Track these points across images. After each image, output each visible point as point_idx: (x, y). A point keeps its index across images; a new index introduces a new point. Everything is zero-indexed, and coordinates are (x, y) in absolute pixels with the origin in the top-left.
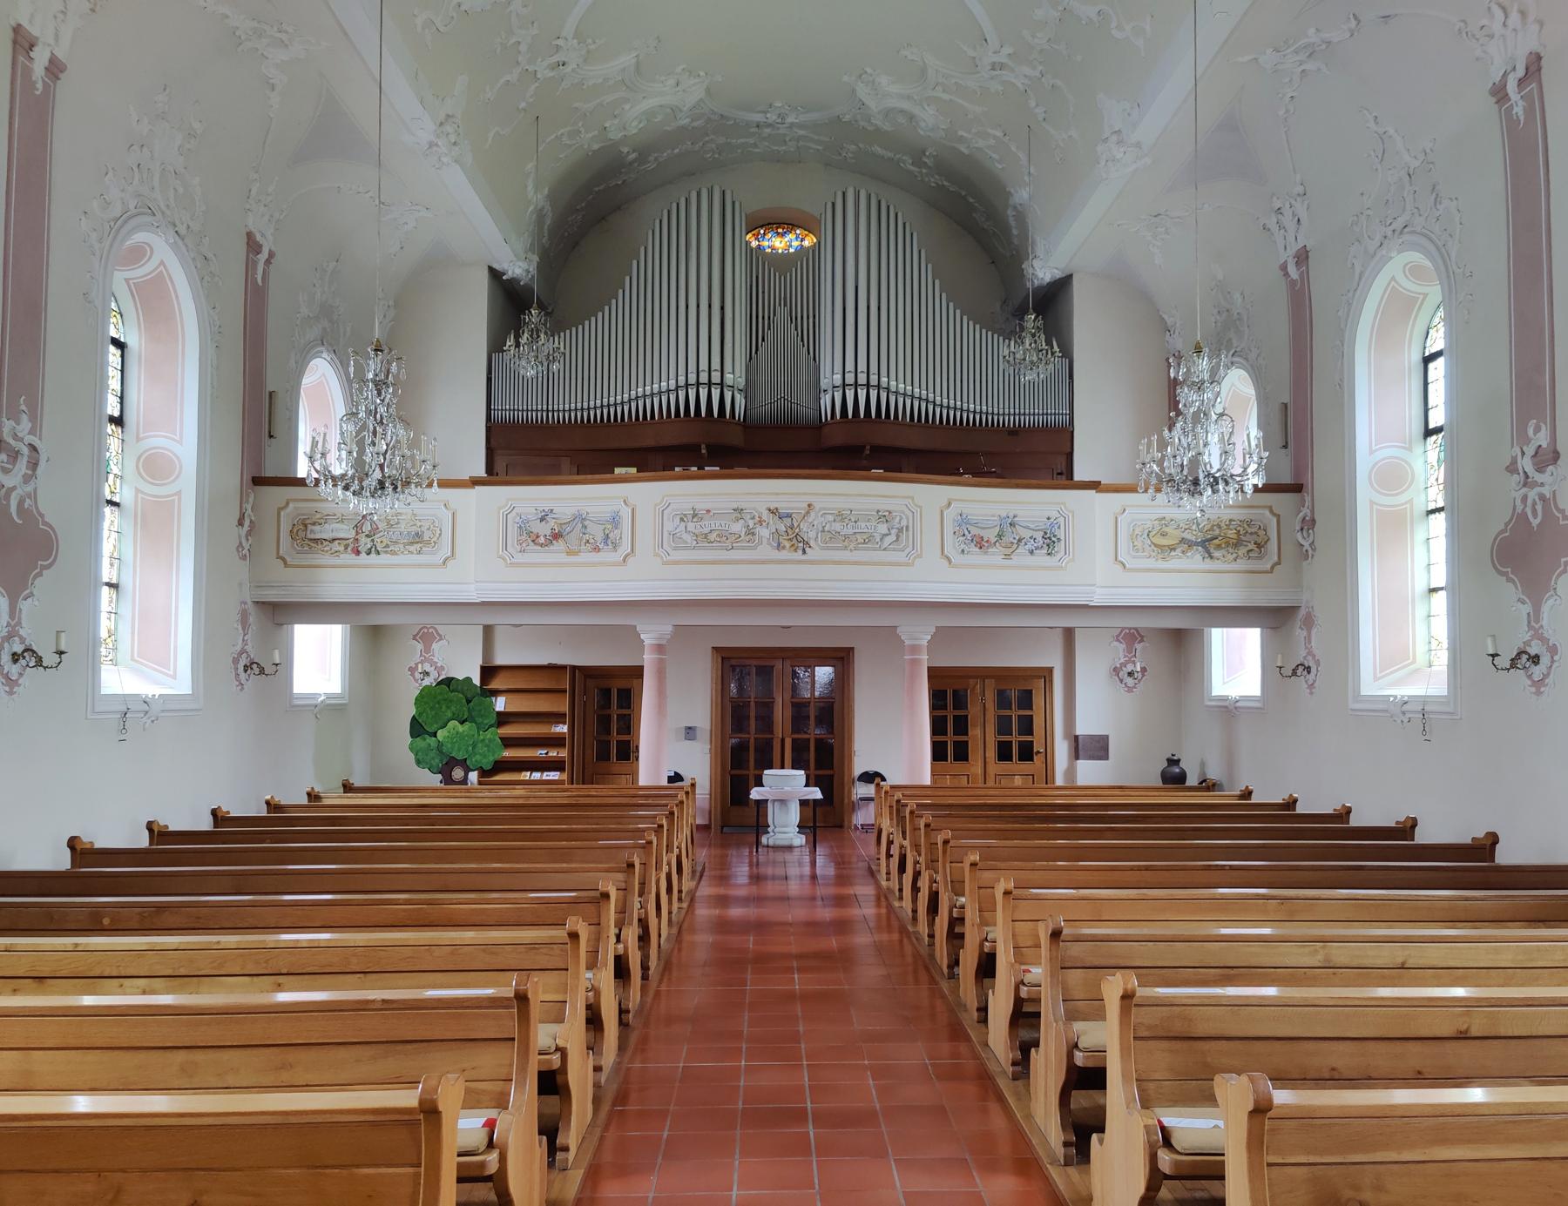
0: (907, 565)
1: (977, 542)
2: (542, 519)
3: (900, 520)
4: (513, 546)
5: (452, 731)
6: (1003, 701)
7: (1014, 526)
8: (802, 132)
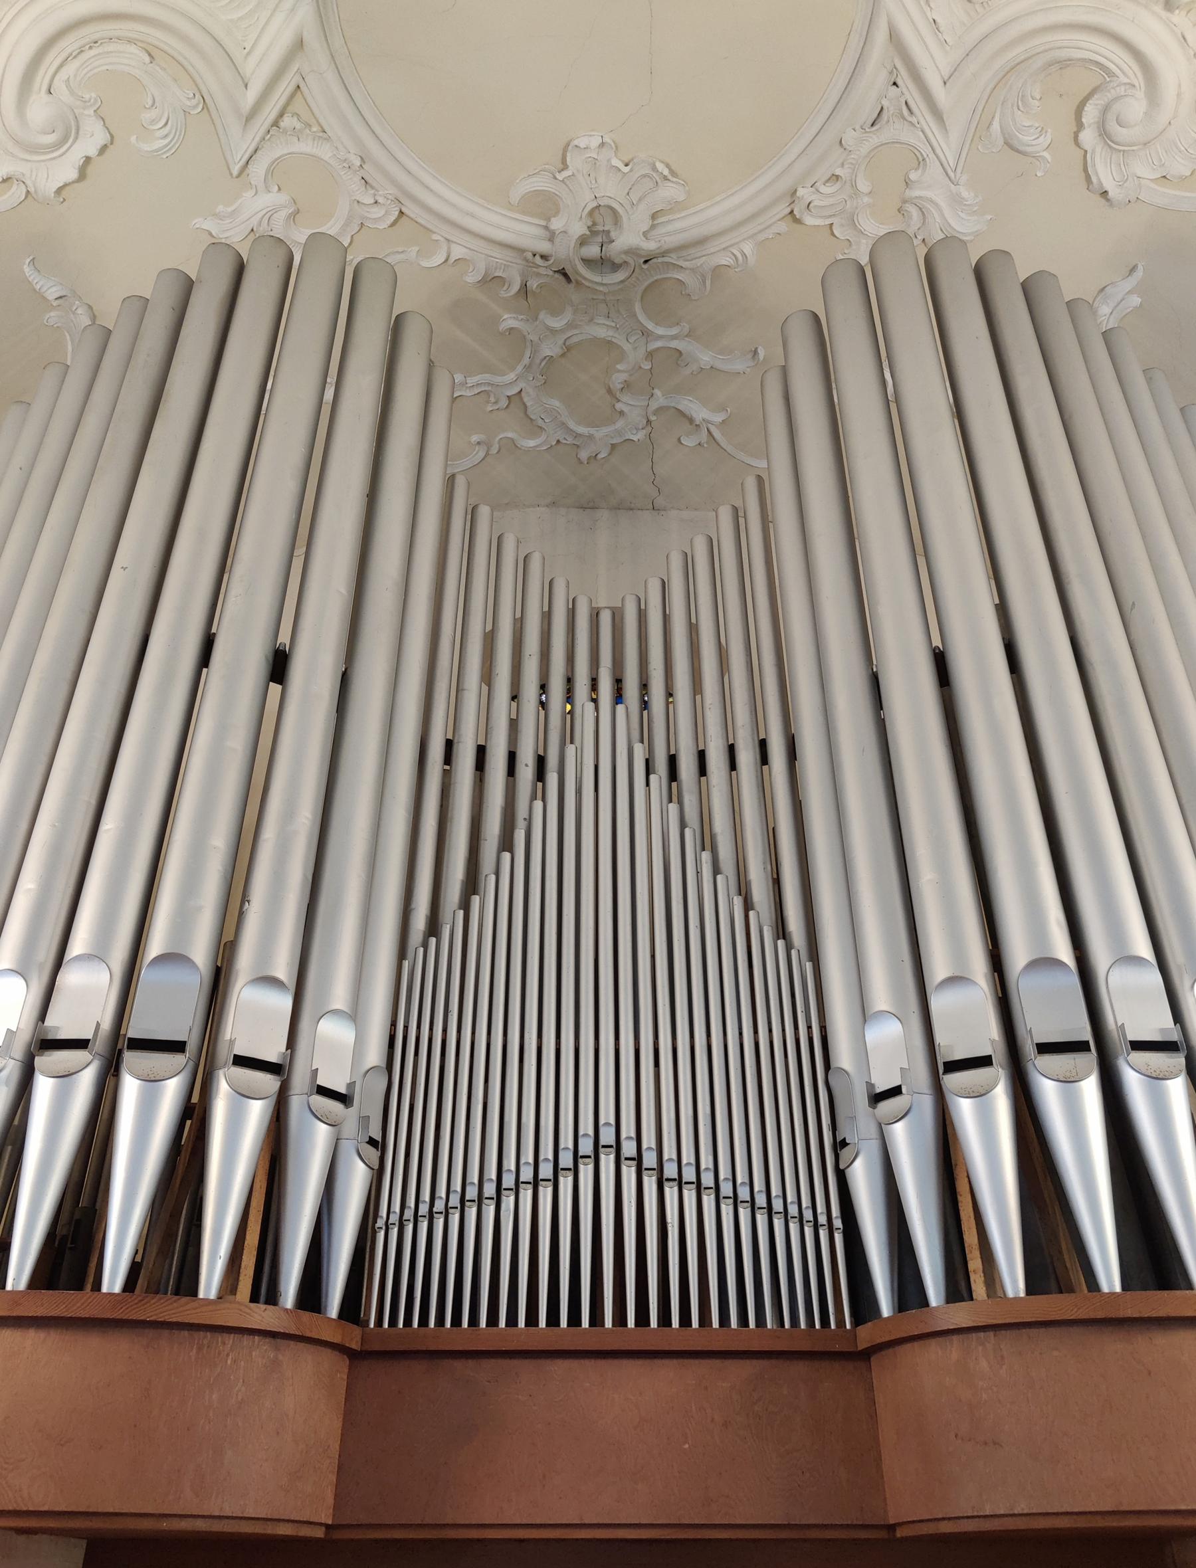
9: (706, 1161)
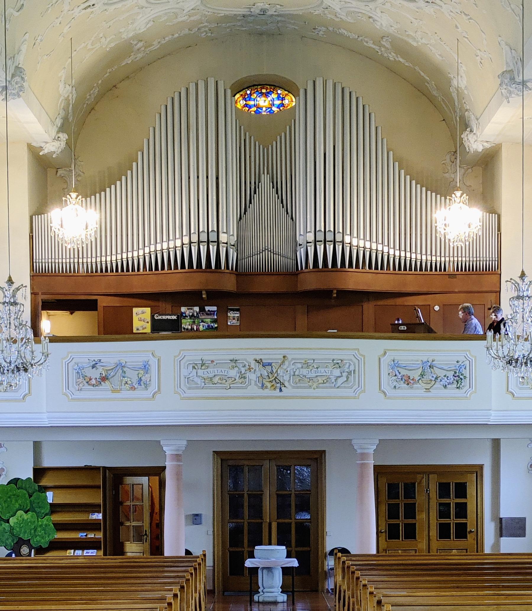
0: (355, 398)
1: (405, 380)
2: (93, 367)
3: (349, 366)
4: (73, 386)
5: (19, 518)
6: (444, 490)
7: (433, 368)
8: (279, 19)
9: (279, 251)
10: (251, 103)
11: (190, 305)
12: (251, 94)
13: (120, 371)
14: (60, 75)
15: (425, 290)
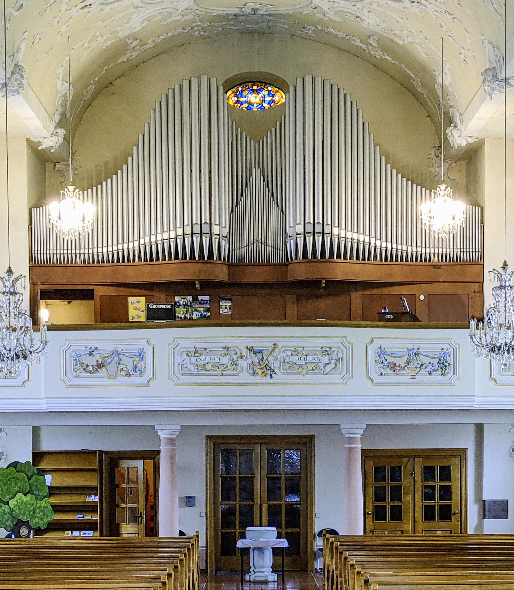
0: (343, 384)
1: (392, 367)
2: (90, 354)
3: (337, 354)
4: (70, 373)
5: (19, 500)
6: (429, 472)
7: (418, 356)
8: (270, 18)
9: (270, 243)
10: (243, 99)
11: (184, 295)
12: (242, 91)
13: (116, 358)
14: (58, 72)
15: (410, 280)
